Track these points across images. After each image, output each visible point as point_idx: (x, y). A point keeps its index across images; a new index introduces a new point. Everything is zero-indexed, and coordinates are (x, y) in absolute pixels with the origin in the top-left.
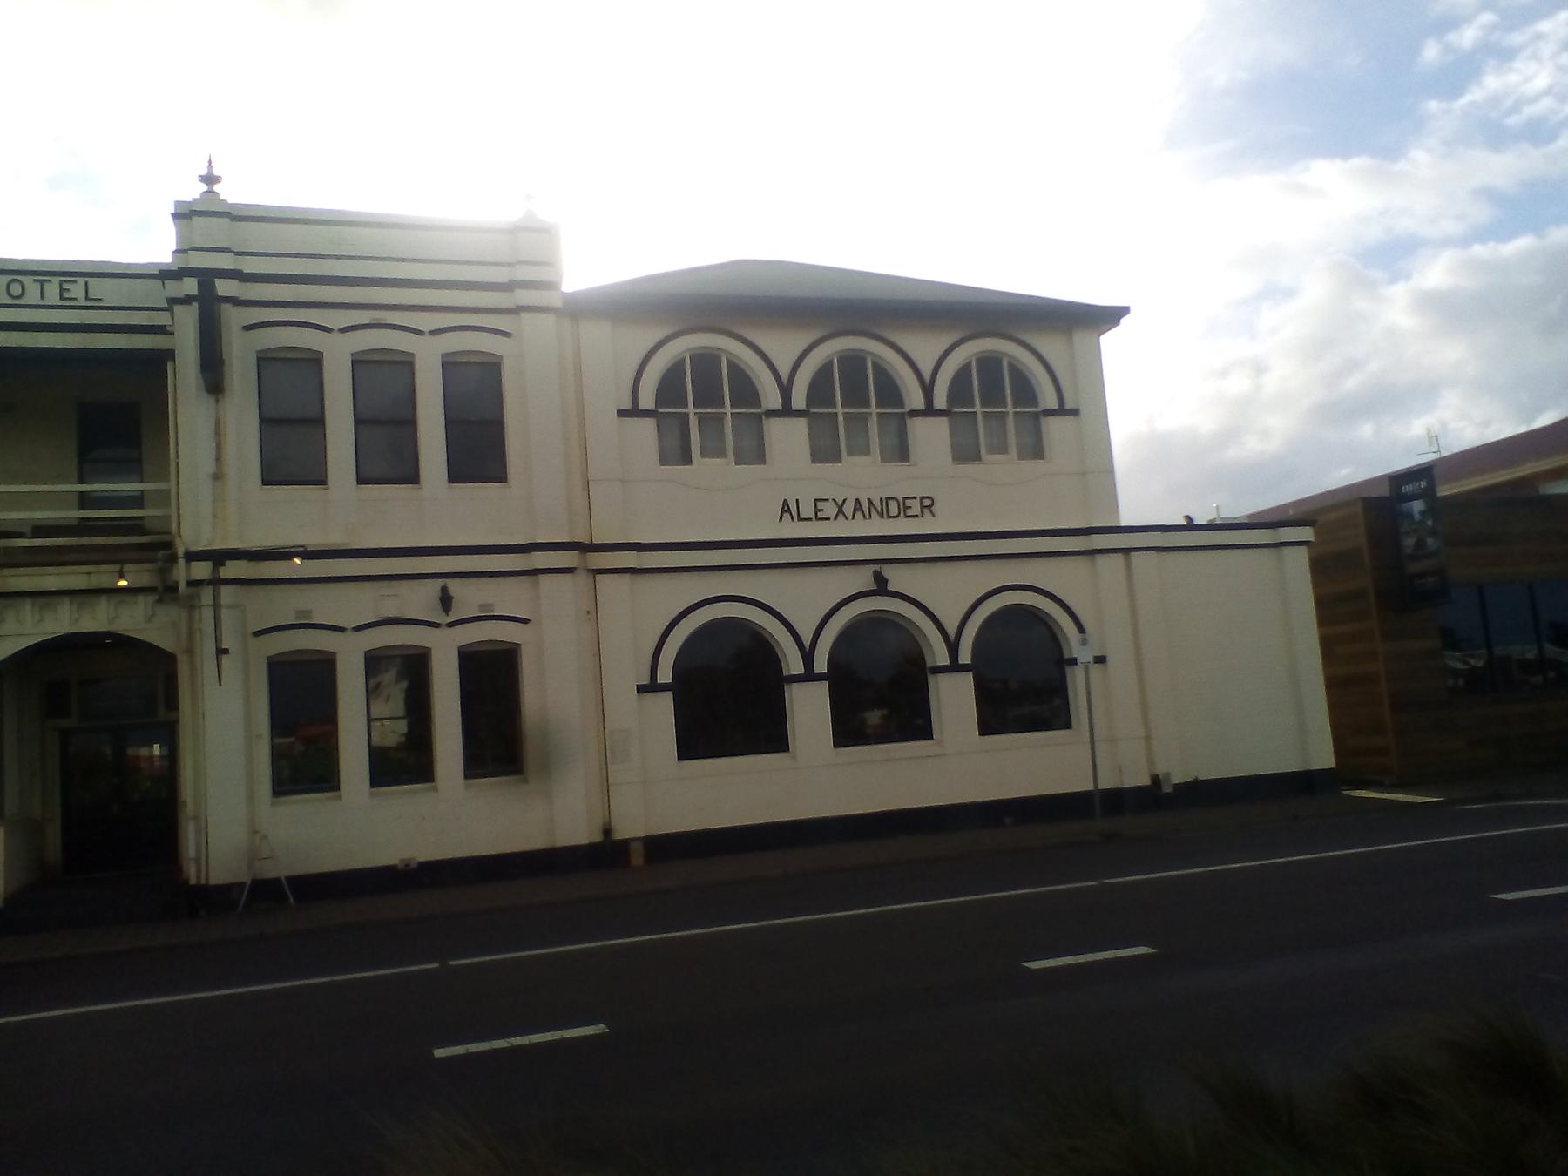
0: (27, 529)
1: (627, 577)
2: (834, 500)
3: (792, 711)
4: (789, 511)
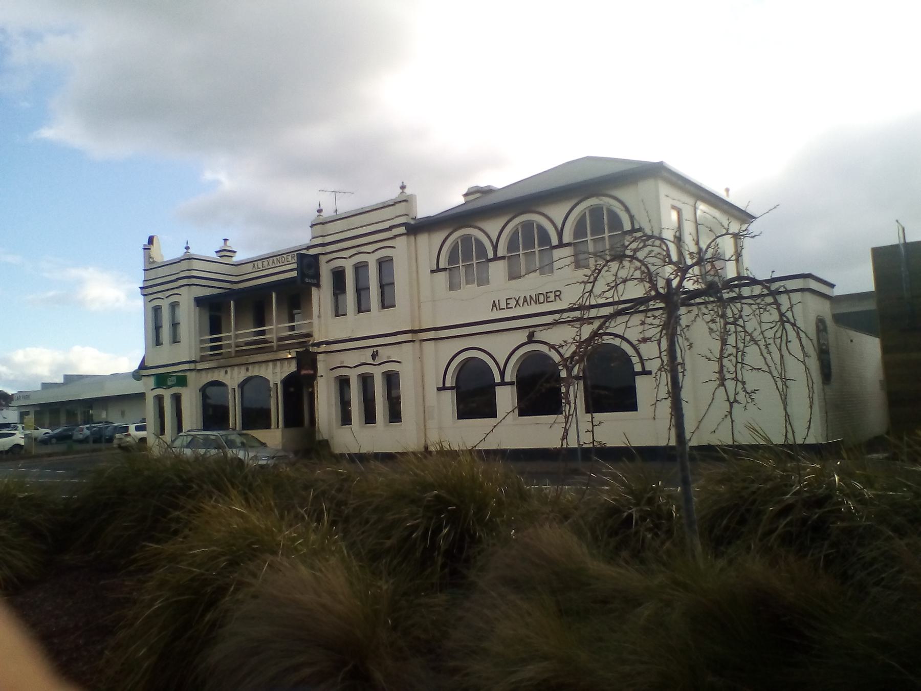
0: (242, 345)
1: (433, 341)
2: (515, 298)
3: (512, 399)
4: (496, 306)
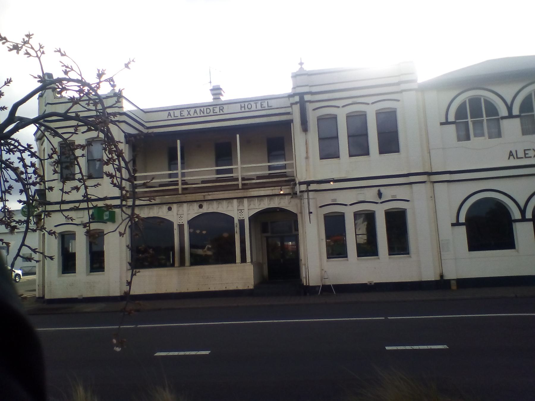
0: (255, 177)
1: (446, 183)
